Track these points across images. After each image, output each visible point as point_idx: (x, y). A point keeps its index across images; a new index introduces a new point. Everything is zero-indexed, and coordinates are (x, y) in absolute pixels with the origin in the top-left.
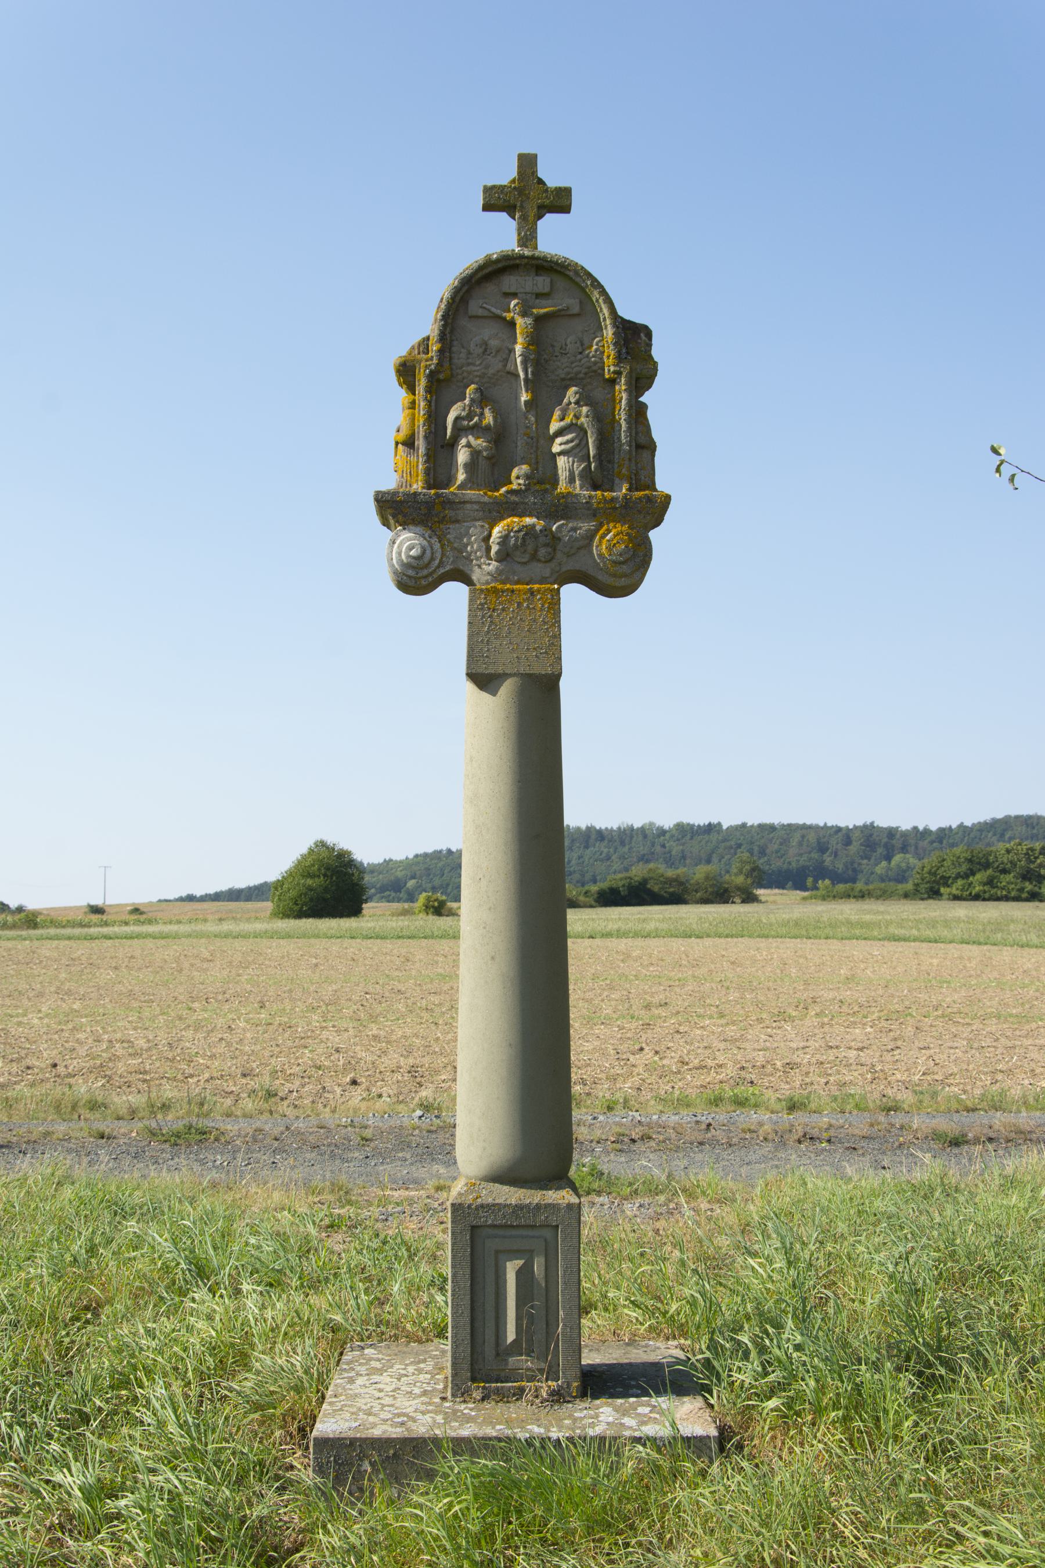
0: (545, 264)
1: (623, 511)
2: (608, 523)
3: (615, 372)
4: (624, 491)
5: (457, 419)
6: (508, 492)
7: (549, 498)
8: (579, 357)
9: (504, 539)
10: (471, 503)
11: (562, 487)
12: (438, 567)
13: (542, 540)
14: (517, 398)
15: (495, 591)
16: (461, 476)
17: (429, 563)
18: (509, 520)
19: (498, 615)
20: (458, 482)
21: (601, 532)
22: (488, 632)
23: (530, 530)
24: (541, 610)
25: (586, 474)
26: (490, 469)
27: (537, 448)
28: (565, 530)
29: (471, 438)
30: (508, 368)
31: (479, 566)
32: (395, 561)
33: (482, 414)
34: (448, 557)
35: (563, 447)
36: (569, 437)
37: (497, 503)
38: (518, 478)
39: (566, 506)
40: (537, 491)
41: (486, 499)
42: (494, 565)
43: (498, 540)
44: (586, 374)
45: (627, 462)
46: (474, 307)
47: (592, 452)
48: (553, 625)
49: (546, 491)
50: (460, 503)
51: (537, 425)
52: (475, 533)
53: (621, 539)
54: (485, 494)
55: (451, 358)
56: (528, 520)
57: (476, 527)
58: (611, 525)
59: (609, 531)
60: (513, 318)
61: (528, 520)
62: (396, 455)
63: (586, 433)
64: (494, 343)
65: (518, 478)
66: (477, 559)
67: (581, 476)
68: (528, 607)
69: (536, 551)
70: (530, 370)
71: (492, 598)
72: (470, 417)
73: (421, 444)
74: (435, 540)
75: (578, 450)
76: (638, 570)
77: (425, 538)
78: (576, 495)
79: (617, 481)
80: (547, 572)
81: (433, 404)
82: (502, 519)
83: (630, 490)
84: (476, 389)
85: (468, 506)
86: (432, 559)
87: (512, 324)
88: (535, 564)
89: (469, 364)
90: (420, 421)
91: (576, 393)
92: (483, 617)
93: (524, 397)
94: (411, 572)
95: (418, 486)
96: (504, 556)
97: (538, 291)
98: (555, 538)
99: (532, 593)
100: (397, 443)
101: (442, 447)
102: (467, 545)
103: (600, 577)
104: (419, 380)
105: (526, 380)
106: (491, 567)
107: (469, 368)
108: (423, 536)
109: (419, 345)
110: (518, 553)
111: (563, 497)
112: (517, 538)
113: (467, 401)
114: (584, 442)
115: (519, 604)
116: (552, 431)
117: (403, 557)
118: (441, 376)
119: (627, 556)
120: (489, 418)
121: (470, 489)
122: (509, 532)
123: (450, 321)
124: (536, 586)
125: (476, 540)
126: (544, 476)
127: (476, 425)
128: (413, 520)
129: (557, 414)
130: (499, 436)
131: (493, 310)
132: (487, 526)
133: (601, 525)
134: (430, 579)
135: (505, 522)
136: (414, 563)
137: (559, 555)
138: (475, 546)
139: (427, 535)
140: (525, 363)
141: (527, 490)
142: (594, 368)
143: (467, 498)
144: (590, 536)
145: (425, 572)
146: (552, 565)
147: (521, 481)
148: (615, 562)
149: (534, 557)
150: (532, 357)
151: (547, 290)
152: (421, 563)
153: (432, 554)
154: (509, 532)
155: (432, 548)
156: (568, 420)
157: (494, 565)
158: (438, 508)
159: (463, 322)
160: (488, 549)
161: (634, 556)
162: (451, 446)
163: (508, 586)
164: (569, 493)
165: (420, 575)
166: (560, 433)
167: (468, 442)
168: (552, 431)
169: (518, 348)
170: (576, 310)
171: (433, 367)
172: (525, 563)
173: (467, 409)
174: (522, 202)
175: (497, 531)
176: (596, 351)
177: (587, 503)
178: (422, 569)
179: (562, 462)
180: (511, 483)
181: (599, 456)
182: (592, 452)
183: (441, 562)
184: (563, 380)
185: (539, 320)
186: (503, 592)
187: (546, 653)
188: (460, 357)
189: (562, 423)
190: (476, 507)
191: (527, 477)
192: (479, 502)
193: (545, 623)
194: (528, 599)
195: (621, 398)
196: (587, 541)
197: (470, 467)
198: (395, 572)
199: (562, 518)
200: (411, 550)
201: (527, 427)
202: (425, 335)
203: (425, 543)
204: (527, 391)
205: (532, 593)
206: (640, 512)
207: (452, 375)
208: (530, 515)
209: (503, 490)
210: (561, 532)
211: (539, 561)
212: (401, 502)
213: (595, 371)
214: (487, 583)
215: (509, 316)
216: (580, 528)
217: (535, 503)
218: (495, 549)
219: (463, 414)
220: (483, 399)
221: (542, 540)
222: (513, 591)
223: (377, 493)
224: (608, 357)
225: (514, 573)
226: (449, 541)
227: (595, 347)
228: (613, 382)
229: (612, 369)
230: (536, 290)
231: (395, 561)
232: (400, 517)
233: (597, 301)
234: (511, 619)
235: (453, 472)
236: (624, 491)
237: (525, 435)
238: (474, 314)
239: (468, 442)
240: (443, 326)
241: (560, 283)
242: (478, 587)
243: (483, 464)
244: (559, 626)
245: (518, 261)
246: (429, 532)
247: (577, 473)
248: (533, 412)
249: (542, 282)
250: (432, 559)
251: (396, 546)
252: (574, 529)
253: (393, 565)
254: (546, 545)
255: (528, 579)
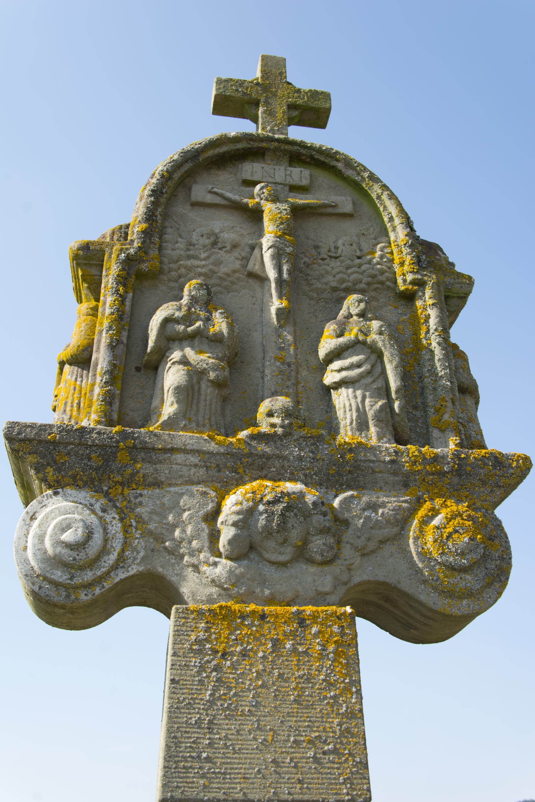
0: (303, 151)
1: (456, 480)
2: (432, 499)
3: (414, 282)
4: (452, 446)
5: (167, 321)
6: (252, 437)
7: (325, 450)
8: (358, 261)
9: (246, 519)
10: (185, 451)
11: (346, 434)
12: (115, 567)
13: (317, 520)
14: (263, 309)
15: (227, 615)
16: (169, 408)
17: (98, 558)
18: (255, 484)
19: (233, 667)
20: (164, 417)
21: (422, 512)
22: (212, 703)
23: (294, 504)
24: (322, 656)
25: (386, 416)
26: (223, 397)
27: (297, 383)
28: (356, 508)
29: (189, 352)
30: (250, 267)
31: (196, 568)
32: (30, 553)
33: (208, 320)
34: (135, 549)
35: (344, 374)
36: (355, 359)
37: (232, 455)
38: (270, 414)
39: (357, 467)
40: (305, 438)
41: (212, 447)
42: (223, 568)
43: (236, 518)
44: (368, 284)
45: (449, 404)
46: (200, 191)
47: (394, 383)
48: (347, 690)
49: (319, 438)
50: (165, 450)
51: (296, 349)
52: (191, 504)
53: (462, 526)
54: (212, 438)
55: (160, 249)
56: (290, 486)
57: (192, 495)
58: (438, 502)
59: (435, 512)
60: (258, 204)
61: (290, 486)
62: (59, 382)
63: (380, 356)
64: (228, 236)
65: (270, 414)
66: (191, 555)
67: (379, 419)
68: (294, 650)
69: (306, 542)
70: (285, 268)
71: (221, 629)
72: (188, 319)
73: (101, 358)
74: (112, 516)
75: (369, 380)
76: (489, 585)
77: (93, 512)
78: (373, 448)
79: (436, 433)
80: (326, 583)
81: (128, 303)
82: (240, 482)
83: (460, 445)
84: (201, 285)
85: (180, 457)
86: (104, 551)
87: (256, 215)
88: (302, 567)
89: (189, 257)
90: (105, 321)
91: (360, 301)
92: (202, 668)
93: (276, 304)
94: (59, 575)
95: (89, 420)
96: (245, 549)
97: (292, 182)
98: (340, 522)
99: (302, 622)
100: (62, 364)
101: (138, 369)
102: (174, 526)
103: (423, 598)
104: (109, 269)
105: (280, 281)
106: (218, 570)
107: (189, 263)
108: (91, 507)
109: (113, 233)
110: (272, 544)
111: (351, 450)
112: (271, 515)
113: (185, 300)
114: (378, 369)
115: (277, 644)
116: (322, 352)
117: (48, 544)
118: (144, 267)
119: (474, 557)
120: (220, 324)
121: (184, 429)
122: (256, 504)
123: (163, 200)
124: (309, 609)
125: (191, 517)
126: (312, 414)
127: (197, 333)
128: (74, 477)
129: (330, 328)
130: (235, 354)
131: (228, 195)
132: (213, 494)
133: (419, 502)
134: (98, 591)
135: (248, 487)
136: (67, 555)
137: (347, 552)
138: (189, 529)
139: (97, 506)
140: (278, 258)
141: (286, 435)
142: (382, 278)
143: (178, 443)
144: (402, 521)
145: (89, 576)
146: (336, 568)
147: (276, 420)
148: (451, 568)
149: (302, 554)
150: (289, 250)
151: (305, 182)
152: (82, 555)
153: (106, 540)
154: (256, 504)
155: (105, 529)
156: (350, 336)
157: (223, 568)
158: (123, 457)
159: (181, 209)
160: (214, 536)
161: (485, 557)
162: (154, 366)
163: (252, 607)
164: (360, 443)
165: (77, 581)
166: (337, 354)
167: (184, 356)
168: (322, 352)
169: (267, 240)
170: (348, 208)
171: (132, 251)
172: (284, 565)
173: (184, 309)
174: (267, 98)
175: (232, 503)
176: (381, 257)
177: (392, 462)
178: (81, 568)
179: (343, 400)
180: (255, 425)
181: (405, 389)
182: (394, 383)
183: (121, 559)
184: (335, 289)
185: (297, 212)
186: (243, 617)
187: (335, 751)
188: (175, 248)
189: (341, 340)
190: (194, 459)
191: (287, 413)
192: (198, 452)
193: (331, 685)
194: (293, 634)
195: (428, 317)
196: (395, 530)
197: (187, 393)
198: (29, 576)
199: (350, 487)
200: (64, 530)
201: (282, 349)
202: (124, 222)
203: (93, 519)
204: (280, 297)
205: (302, 622)
206: (484, 483)
207: (161, 271)
208: (293, 479)
209: (243, 434)
210: (349, 510)
211: (311, 561)
212: (54, 443)
213: (382, 283)
214: (210, 600)
215: (251, 203)
216: (383, 505)
217: (300, 459)
218: (227, 533)
219: (177, 314)
220: (208, 301)
221: (317, 520)
222: (263, 617)
223: (12, 426)
224: (402, 264)
225: (263, 583)
226: (140, 519)
227: (378, 253)
228: (409, 298)
229: (410, 277)
230: (289, 181)
231: (30, 553)
232: (50, 471)
233: (379, 197)
234: (259, 675)
235: (156, 403)
236: (452, 446)
237: (277, 359)
238: (200, 199)
239: (184, 356)
240: (153, 203)
241: (324, 178)
242: (192, 606)
243: (207, 391)
244: (359, 692)
245: (264, 145)
246: (103, 501)
247: (370, 414)
248: (290, 328)
249: (299, 175)
250: (104, 551)
251: (36, 523)
252: (373, 507)
253: (26, 561)
254: (324, 531)
255: (290, 595)
